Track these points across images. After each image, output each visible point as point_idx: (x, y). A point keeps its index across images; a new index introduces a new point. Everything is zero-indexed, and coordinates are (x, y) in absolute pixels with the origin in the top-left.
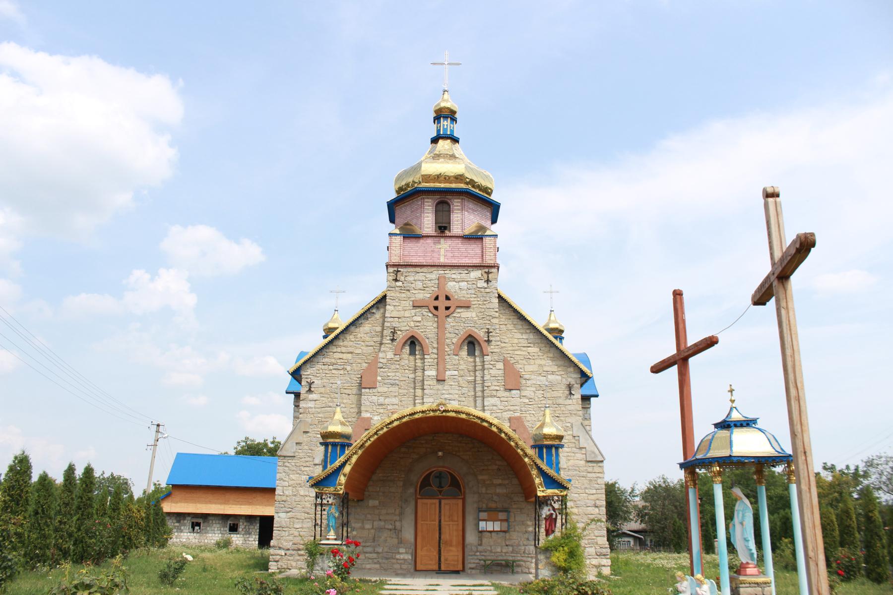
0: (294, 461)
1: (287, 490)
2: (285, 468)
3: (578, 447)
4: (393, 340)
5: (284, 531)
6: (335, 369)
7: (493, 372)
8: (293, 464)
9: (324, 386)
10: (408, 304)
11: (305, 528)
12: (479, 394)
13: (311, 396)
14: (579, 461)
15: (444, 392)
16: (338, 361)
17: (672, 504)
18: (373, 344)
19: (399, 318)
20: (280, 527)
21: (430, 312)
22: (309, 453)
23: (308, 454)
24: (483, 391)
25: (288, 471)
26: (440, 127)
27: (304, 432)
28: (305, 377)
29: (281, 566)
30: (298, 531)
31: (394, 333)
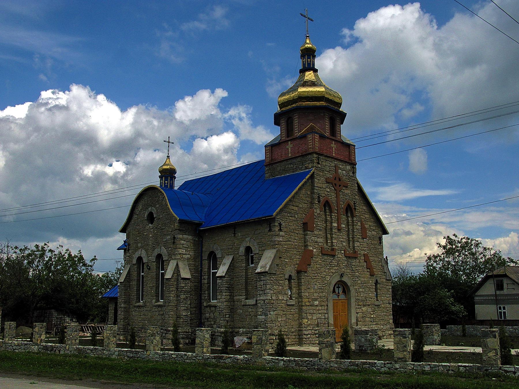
0: (275, 277)
1: (273, 296)
3: (383, 272)
4: (319, 202)
5: (273, 323)
8: (275, 278)
12: (351, 239)
14: (383, 279)
17: (50, 368)
19: (320, 188)
20: (271, 321)
21: (333, 186)
24: (353, 238)
28: (277, 220)
29: (274, 346)
31: (319, 197)
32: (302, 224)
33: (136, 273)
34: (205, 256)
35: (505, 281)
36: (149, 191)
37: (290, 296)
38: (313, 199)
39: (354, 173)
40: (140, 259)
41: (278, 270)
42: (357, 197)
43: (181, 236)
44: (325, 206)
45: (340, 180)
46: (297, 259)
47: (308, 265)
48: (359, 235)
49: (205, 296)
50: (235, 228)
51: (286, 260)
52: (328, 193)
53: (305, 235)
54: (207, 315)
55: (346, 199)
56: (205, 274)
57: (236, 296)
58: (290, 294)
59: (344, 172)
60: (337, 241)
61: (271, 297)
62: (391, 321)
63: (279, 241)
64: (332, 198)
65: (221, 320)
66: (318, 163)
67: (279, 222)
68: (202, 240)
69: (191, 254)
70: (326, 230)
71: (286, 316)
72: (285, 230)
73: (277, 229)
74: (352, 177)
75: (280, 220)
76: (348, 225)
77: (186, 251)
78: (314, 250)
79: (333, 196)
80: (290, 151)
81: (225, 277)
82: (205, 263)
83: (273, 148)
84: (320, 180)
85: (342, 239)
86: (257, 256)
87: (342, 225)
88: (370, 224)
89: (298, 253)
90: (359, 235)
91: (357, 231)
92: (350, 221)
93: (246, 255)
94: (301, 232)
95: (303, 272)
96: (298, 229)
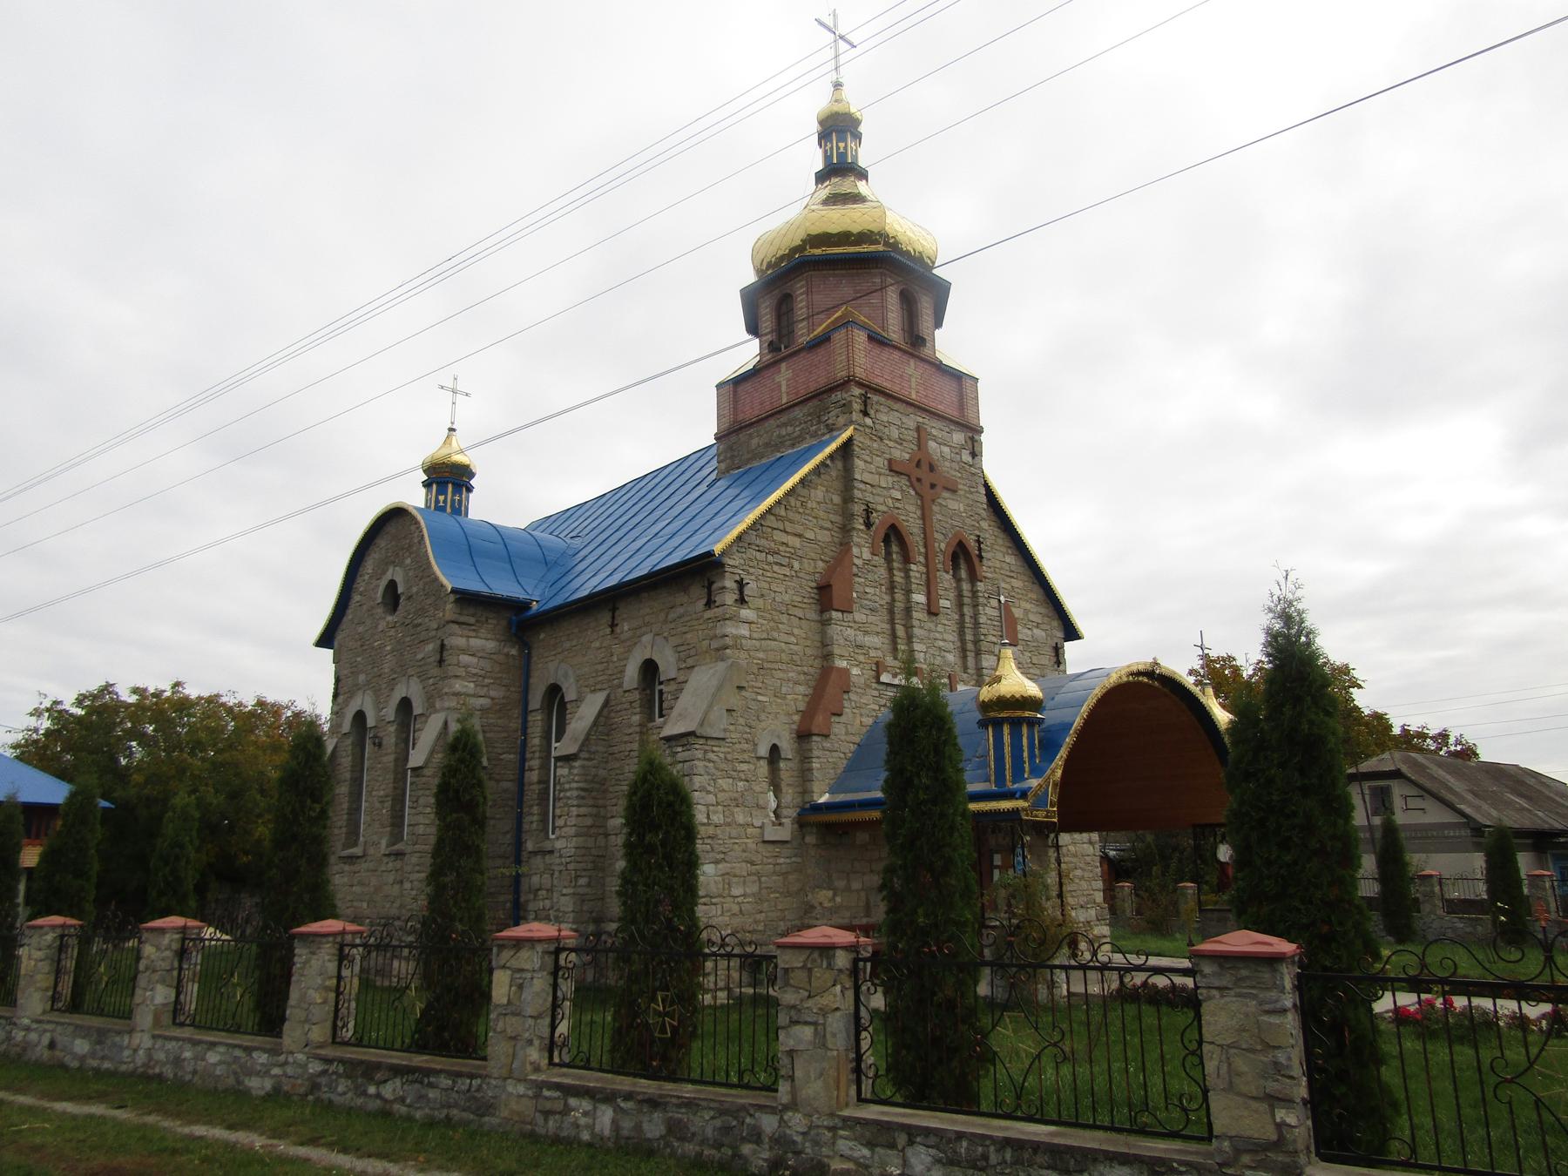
0: (722, 749)
1: (716, 812)
2: (707, 764)
4: (868, 525)
6: (777, 563)
7: (989, 611)
8: (722, 755)
9: (762, 595)
10: (880, 462)
11: (749, 896)
12: (970, 646)
13: (746, 613)
15: (937, 635)
16: (781, 548)
18: (828, 525)
19: (872, 486)
22: (746, 733)
23: (745, 736)
25: (713, 771)
26: (832, 148)
27: (738, 687)
28: (731, 570)
30: (738, 903)
31: (868, 512)
32: (815, 591)
33: (350, 758)
34: (536, 700)
35: (1398, 790)
36: (394, 517)
37: (775, 812)
38: (848, 516)
39: (975, 454)
40: (360, 717)
41: (731, 728)
42: (984, 524)
43: (460, 642)
44: (887, 540)
45: (932, 468)
46: (797, 696)
47: (834, 714)
48: (995, 633)
49: (532, 822)
50: (614, 610)
51: (760, 698)
52: (897, 505)
53: (825, 623)
54: (535, 879)
55: (953, 526)
56: (533, 752)
57: (612, 817)
58: (773, 805)
59: (946, 450)
60: (927, 648)
61: (708, 814)
62: (1099, 897)
63: (736, 637)
64: (911, 523)
65: (564, 895)
66: (865, 413)
67: (738, 578)
68: (529, 653)
69: (492, 693)
70: (891, 612)
71: (760, 880)
72: (760, 603)
73: (730, 598)
74: (971, 466)
75: (741, 572)
76: (960, 605)
77: (476, 686)
78: (855, 671)
79: (911, 515)
80: (784, 389)
81: (580, 758)
82: (536, 721)
83: (740, 389)
84: (871, 463)
85: (941, 644)
86: (672, 687)
87: (941, 601)
88: (1027, 608)
89: (802, 677)
90: (995, 633)
91: (989, 622)
92: (966, 593)
93: (644, 690)
94: (813, 615)
95: (818, 735)
96: (800, 605)
